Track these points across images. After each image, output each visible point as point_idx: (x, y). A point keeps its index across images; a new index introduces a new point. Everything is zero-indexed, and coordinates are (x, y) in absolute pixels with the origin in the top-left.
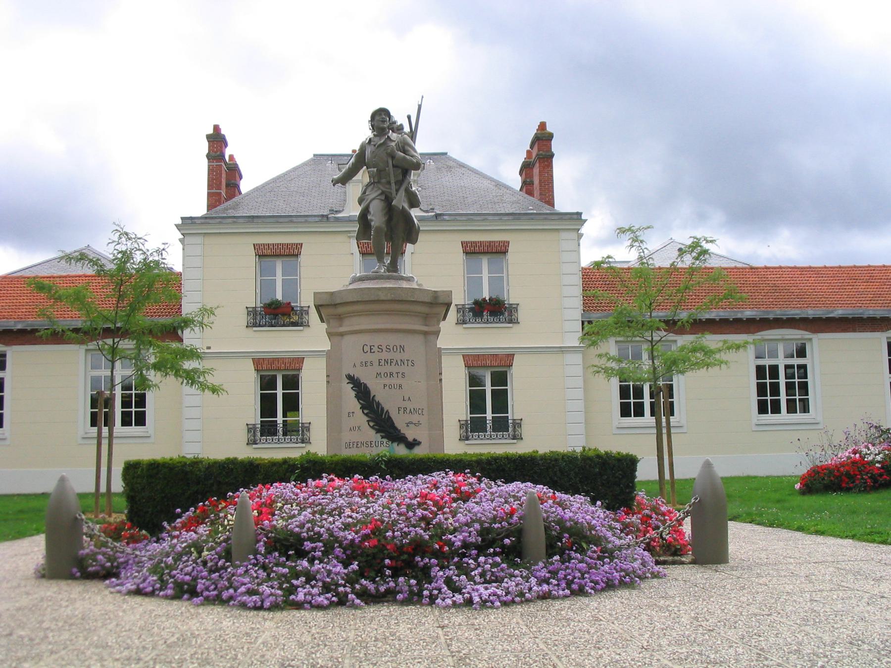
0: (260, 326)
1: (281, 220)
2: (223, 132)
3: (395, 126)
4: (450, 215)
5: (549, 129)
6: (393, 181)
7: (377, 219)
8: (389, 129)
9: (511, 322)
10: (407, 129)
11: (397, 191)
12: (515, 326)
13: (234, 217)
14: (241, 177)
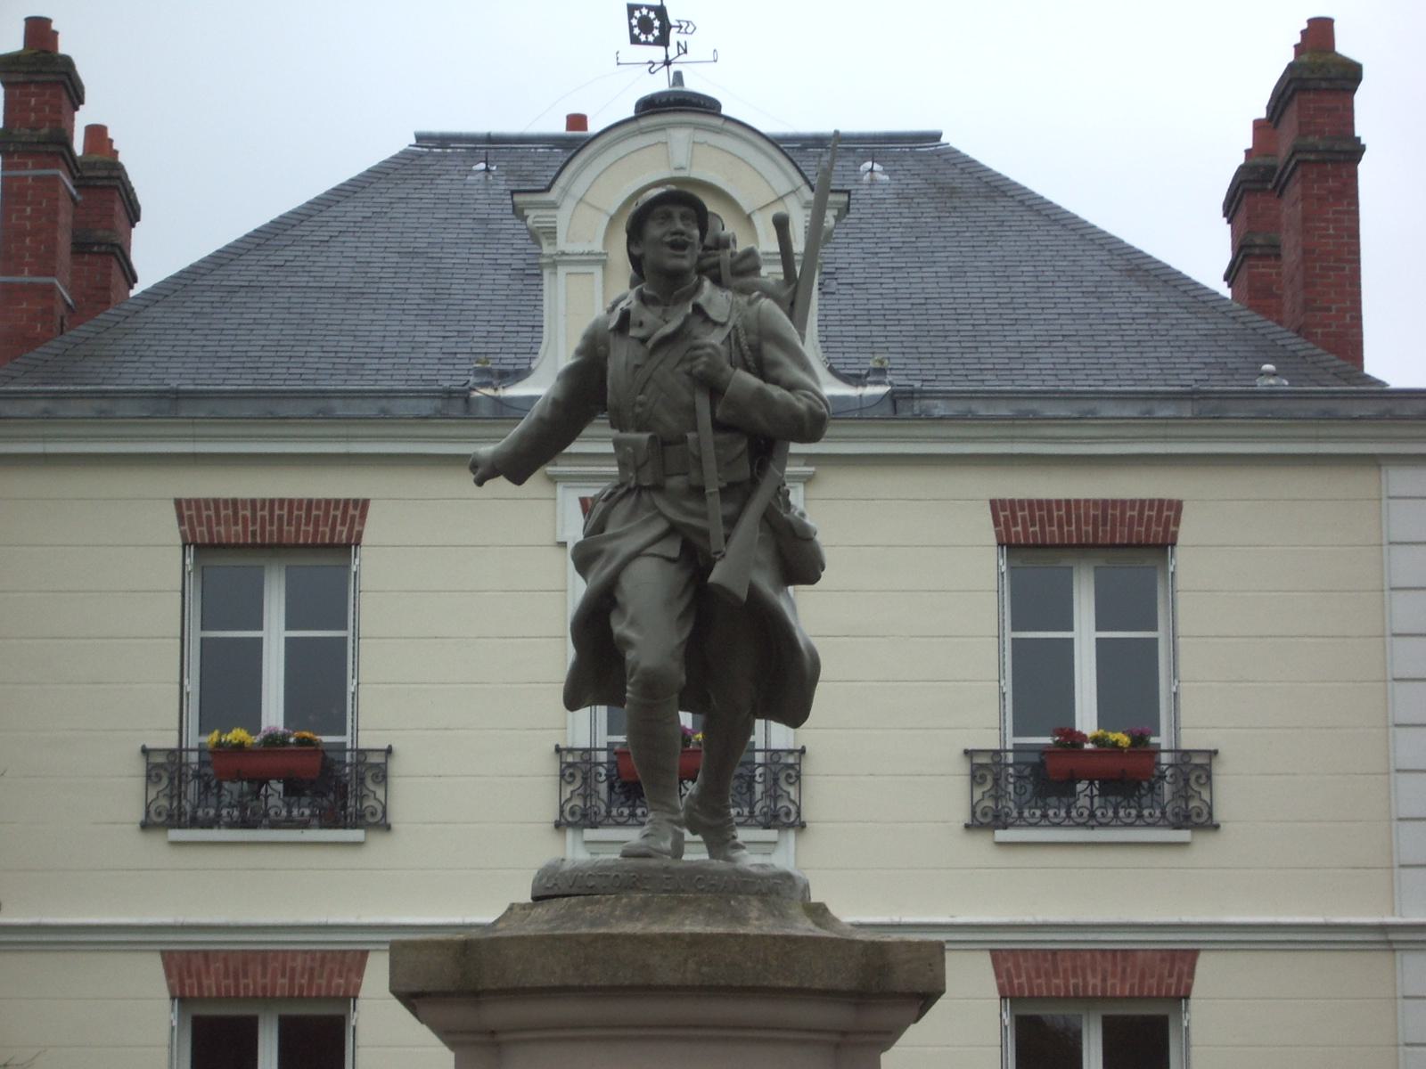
0: (195, 823)
1: (286, 408)
2: (63, 48)
3: (725, 256)
4: (948, 396)
5: (1345, 46)
6: (712, 489)
7: (651, 637)
8: (702, 271)
9: (1184, 820)
10: (771, 272)
11: (731, 522)
12: (1203, 841)
13: (104, 395)
14: (133, 214)
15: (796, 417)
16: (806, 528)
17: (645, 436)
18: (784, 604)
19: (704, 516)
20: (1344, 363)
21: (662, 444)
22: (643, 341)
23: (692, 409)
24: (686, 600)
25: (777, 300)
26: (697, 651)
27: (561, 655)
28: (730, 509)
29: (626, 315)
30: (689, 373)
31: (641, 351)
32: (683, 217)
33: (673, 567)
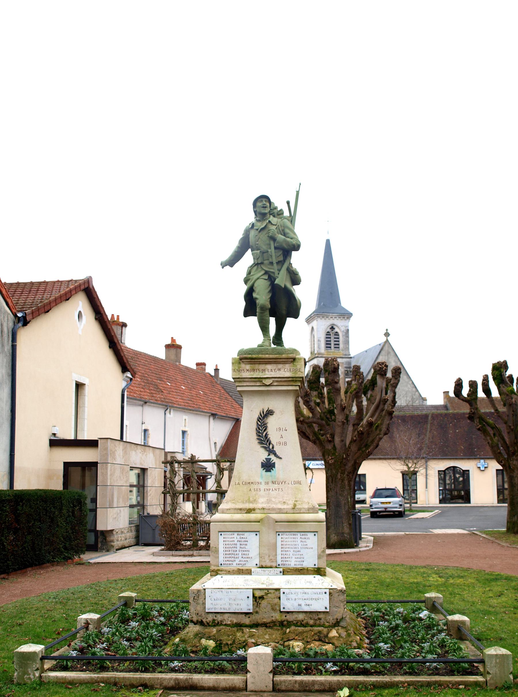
6: (274, 262)
10: (286, 213)
11: (279, 270)
15: (294, 245)
16: (297, 272)
17: (259, 251)
18: (292, 289)
19: (273, 269)
20: (218, 450)
21: (263, 253)
22: (257, 230)
23: (270, 245)
24: (269, 289)
25: (288, 220)
26: (273, 300)
27: (242, 304)
28: (279, 267)
29: (253, 224)
30: (268, 236)
31: (257, 232)
32: (265, 201)
33: (266, 281)
